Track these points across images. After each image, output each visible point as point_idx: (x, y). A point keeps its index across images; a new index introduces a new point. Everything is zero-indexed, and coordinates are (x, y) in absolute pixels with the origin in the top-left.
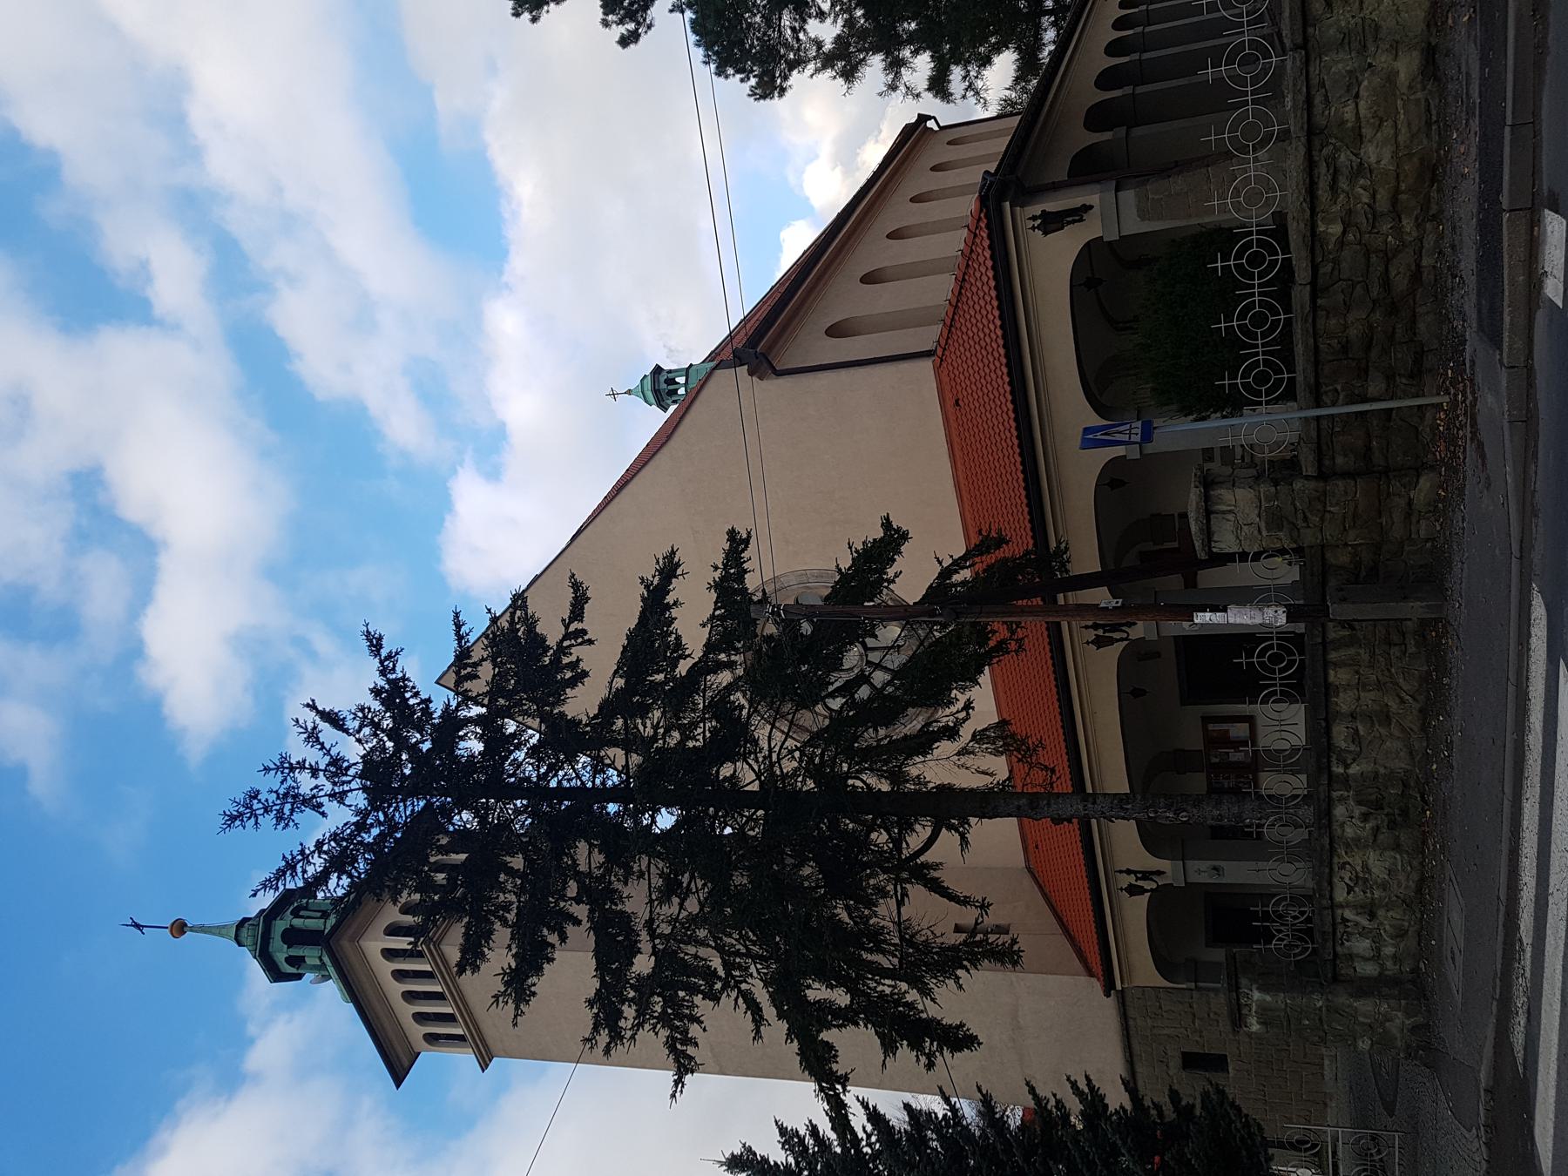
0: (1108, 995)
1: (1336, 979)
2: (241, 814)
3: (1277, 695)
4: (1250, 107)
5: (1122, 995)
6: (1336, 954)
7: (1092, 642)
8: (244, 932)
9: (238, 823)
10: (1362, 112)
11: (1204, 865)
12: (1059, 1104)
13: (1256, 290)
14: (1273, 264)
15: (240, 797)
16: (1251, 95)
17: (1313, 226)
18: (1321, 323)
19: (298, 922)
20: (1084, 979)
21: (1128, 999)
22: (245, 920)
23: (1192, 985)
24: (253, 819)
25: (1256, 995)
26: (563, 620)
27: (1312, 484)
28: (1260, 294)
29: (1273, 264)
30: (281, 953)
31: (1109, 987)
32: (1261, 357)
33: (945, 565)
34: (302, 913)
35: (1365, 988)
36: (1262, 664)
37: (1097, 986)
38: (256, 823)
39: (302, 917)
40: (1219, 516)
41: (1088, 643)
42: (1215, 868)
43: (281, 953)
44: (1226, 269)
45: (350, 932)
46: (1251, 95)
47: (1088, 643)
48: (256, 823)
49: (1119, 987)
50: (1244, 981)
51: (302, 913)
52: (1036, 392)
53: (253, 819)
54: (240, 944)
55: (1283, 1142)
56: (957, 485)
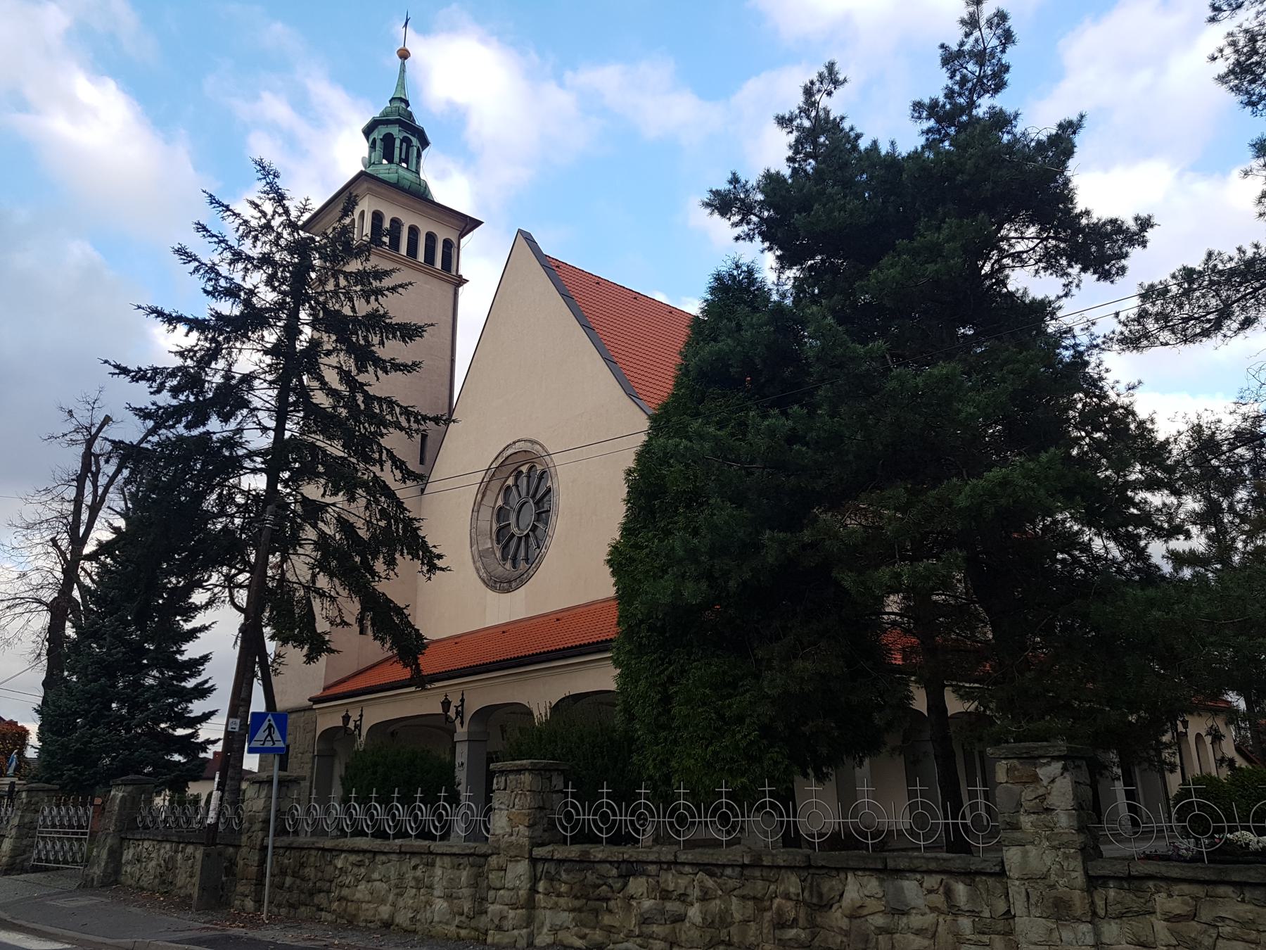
0: (310, 700)
1: (123, 839)
2: (264, 170)
3: (734, 817)
4: (950, 821)
5: (310, 709)
6: (130, 839)
7: (446, 699)
8: (397, 104)
9: (258, 168)
10: (376, 883)
11: (464, 760)
12: (199, 673)
13: (841, 820)
14: (601, 830)
15: (274, 167)
16: (1162, 823)
17: (342, 851)
18: (313, 852)
19: (397, 143)
20: (322, 684)
21: (307, 713)
22: (408, 104)
23: (316, 753)
24: (263, 176)
25: (121, 795)
26: (393, 359)
27: (259, 842)
28: (621, 820)
29: (601, 830)
30: (378, 134)
31: (316, 700)
32: (785, 819)
33: (405, 611)
34: (404, 144)
35: (115, 855)
36: (601, 805)
37: (317, 692)
38: (261, 179)
39: (401, 145)
40: (257, 789)
41: (446, 696)
42: (462, 764)
43: (378, 134)
44: (720, 795)
45: (373, 187)
46: (1162, 823)
47: (446, 696)
48: (261, 179)
49: (315, 707)
50: (129, 788)
51: (404, 144)
52: (553, 667)
53: (263, 176)
54: (390, 101)
55: (329, 802)
56: (593, 603)
